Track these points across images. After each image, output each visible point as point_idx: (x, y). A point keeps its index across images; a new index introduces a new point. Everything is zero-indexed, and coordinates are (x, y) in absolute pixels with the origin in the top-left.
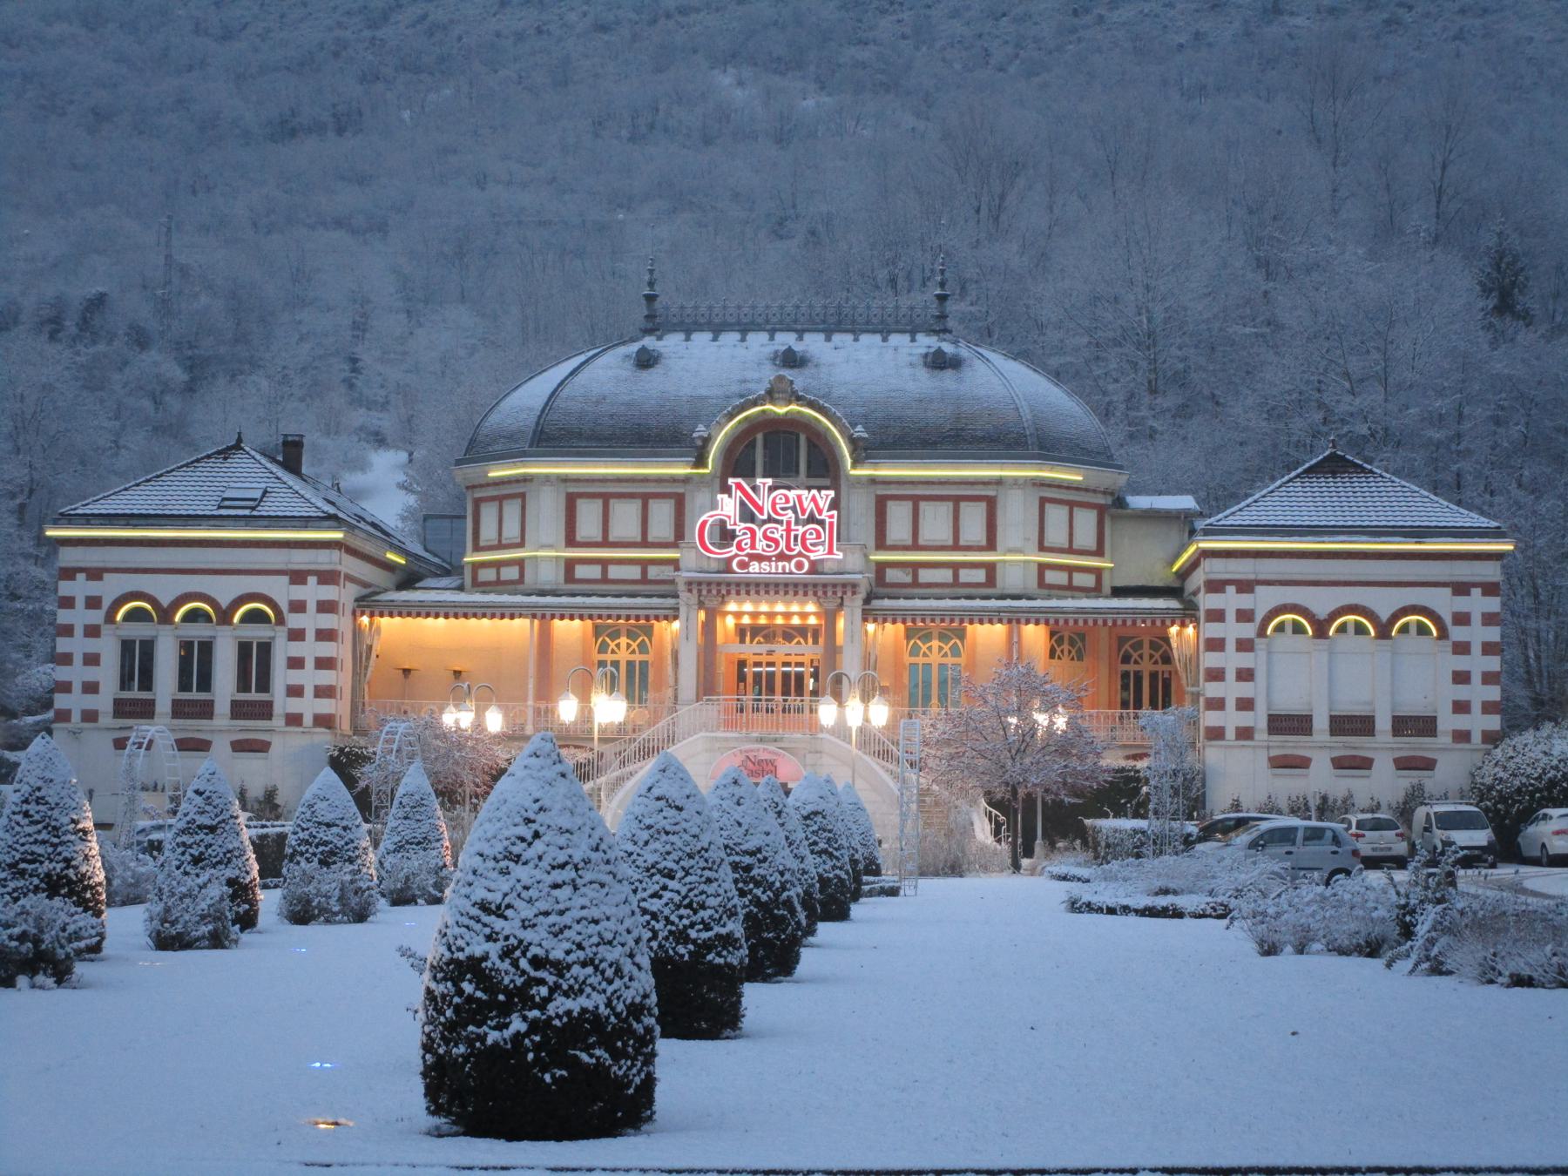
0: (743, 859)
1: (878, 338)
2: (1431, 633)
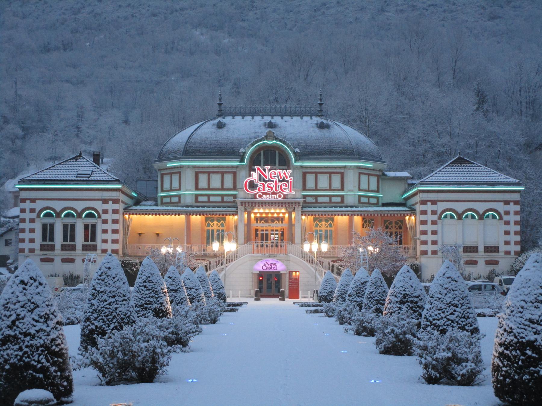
0: (414, 299)
1: (299, 118)
2: (455, 218)
